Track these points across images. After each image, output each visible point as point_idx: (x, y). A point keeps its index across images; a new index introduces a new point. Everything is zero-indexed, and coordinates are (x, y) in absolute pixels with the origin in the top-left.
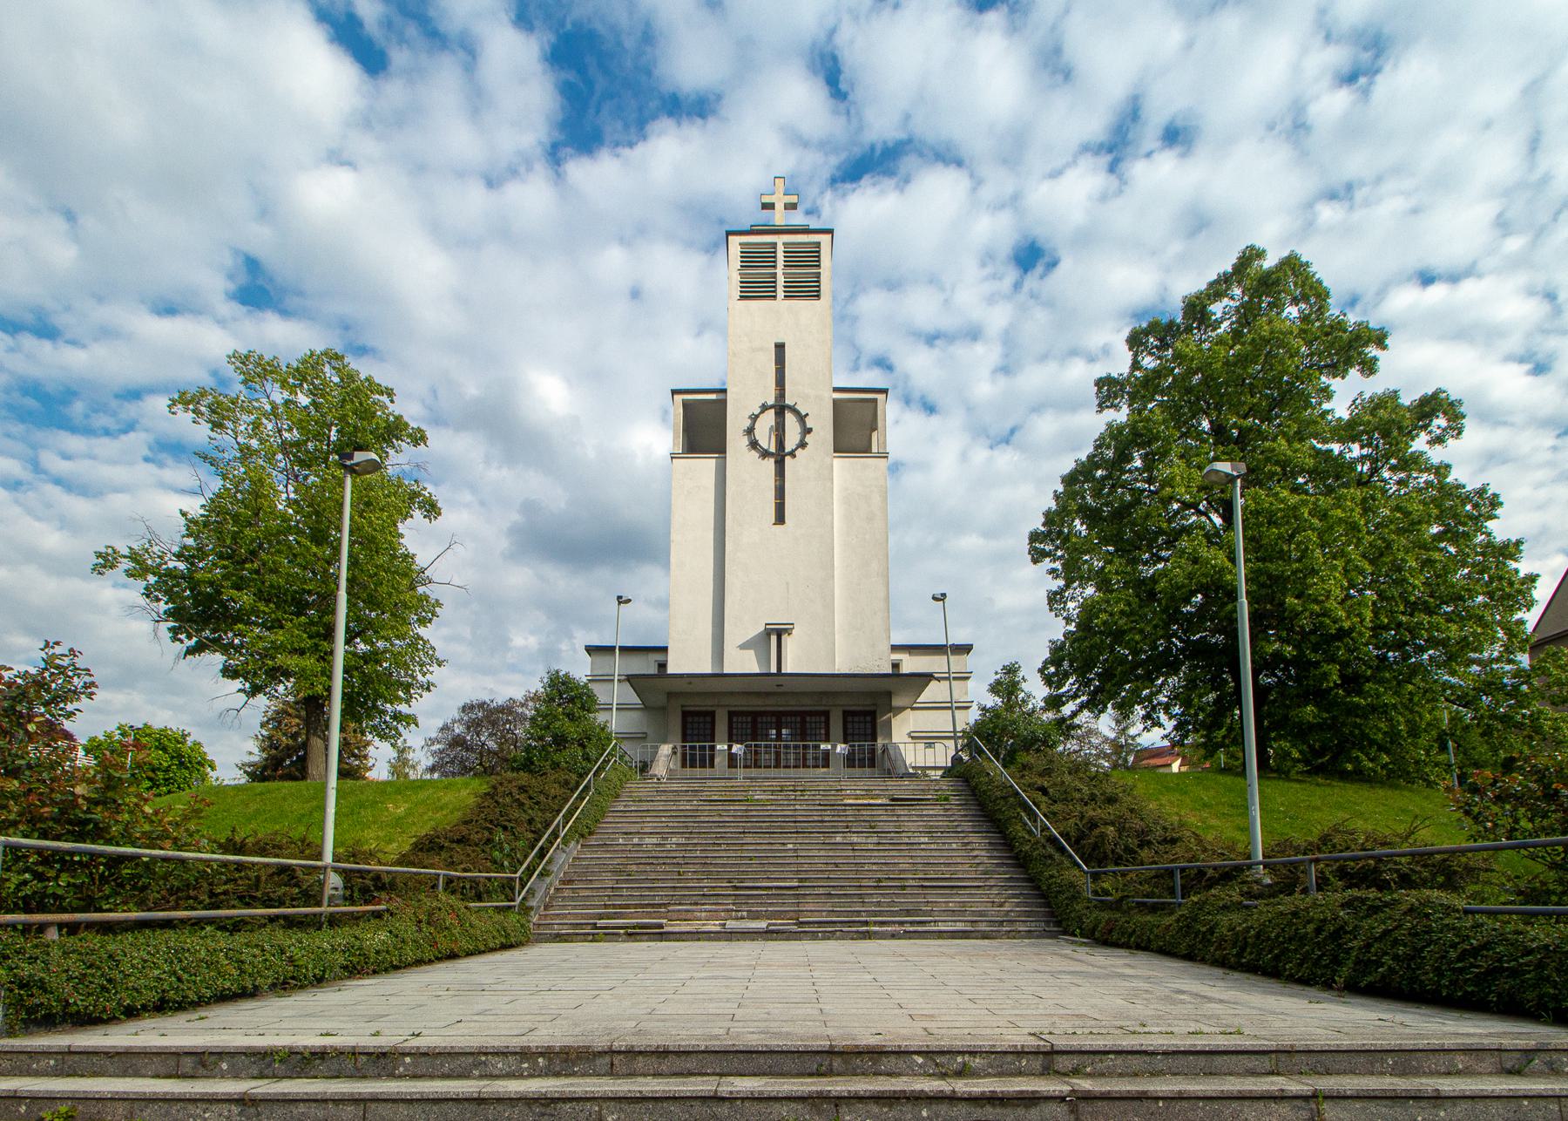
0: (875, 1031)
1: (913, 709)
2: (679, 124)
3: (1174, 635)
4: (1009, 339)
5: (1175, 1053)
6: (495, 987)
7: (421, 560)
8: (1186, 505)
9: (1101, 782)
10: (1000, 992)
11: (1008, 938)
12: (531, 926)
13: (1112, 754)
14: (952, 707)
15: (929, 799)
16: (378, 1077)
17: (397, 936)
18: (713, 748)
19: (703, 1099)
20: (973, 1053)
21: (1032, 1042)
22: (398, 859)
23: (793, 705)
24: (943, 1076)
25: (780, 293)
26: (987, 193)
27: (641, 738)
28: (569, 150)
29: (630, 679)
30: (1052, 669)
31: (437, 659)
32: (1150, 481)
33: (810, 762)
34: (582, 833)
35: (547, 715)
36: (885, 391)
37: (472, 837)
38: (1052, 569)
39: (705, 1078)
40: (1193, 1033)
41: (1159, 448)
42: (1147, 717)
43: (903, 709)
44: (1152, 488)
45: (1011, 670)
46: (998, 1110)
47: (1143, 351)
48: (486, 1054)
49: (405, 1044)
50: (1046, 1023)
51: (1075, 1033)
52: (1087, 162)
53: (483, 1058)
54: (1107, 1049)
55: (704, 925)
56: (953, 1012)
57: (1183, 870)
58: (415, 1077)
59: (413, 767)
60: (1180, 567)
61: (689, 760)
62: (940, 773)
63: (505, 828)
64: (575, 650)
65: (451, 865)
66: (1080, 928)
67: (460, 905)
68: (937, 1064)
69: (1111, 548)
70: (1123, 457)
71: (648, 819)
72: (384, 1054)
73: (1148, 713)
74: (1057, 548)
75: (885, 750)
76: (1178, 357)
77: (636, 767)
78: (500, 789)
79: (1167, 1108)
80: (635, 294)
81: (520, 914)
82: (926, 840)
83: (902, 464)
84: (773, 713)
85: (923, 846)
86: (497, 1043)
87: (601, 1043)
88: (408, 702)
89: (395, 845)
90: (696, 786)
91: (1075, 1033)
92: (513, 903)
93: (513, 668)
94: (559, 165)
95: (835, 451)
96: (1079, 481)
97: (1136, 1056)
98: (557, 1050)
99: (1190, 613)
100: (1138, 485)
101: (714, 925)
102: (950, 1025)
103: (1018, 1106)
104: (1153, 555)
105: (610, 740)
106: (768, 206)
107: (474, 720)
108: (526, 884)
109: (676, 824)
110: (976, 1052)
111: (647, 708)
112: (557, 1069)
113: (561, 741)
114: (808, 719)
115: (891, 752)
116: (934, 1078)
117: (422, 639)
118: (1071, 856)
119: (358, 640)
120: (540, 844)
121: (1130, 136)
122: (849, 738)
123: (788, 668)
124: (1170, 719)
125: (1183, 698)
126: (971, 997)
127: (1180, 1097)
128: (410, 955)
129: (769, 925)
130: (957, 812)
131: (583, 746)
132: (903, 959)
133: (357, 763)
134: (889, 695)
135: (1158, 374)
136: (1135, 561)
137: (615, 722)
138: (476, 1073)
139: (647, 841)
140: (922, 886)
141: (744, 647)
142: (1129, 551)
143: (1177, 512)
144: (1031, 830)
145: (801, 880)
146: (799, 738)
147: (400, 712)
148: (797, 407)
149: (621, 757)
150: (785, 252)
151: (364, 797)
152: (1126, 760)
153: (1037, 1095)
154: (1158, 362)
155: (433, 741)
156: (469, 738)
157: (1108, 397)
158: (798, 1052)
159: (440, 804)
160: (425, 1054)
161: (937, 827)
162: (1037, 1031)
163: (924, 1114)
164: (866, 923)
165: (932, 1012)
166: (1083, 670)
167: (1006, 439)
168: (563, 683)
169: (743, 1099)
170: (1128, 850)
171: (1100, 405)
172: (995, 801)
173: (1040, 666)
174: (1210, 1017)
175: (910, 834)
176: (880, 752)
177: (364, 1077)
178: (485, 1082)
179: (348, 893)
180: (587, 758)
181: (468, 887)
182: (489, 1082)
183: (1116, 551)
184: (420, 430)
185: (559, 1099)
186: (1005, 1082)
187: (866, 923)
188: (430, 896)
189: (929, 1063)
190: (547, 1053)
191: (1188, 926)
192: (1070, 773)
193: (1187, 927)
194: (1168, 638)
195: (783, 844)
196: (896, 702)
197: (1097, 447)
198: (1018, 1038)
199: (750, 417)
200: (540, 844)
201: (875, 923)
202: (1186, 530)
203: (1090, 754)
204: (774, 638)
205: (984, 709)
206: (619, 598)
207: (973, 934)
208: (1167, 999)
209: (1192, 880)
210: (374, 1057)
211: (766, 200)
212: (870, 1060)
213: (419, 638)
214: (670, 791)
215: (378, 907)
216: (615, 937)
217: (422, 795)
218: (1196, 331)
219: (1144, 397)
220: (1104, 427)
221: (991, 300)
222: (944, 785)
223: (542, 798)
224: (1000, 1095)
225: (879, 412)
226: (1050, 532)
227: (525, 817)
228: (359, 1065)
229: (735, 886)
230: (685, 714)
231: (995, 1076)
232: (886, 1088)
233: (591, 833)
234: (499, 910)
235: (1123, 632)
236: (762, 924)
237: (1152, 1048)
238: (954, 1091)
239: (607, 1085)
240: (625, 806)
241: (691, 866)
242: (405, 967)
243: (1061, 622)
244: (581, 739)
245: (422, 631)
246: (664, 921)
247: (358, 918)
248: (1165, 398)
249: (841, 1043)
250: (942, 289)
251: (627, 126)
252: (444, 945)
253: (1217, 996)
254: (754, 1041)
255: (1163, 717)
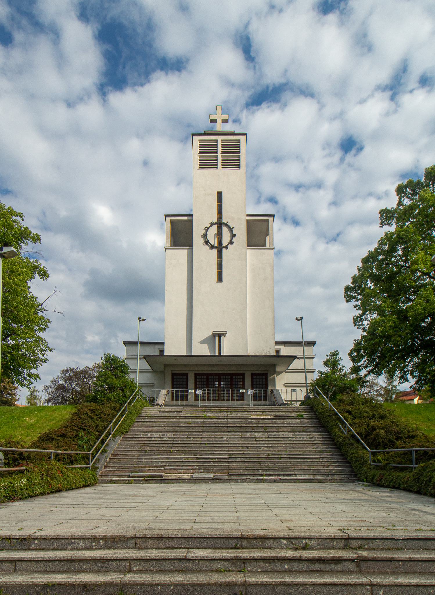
0: (263, 528)
1: (286, 372)
2: (167, 74)
3: (416, 337)
4: (337, 188)
5: (408, 539)
6: (79, 506)
7: (40, 300)
8: (424, 274)
9: (378, 408)
10: (325, 509)
11: (331, 482)
12: (98, 476)
13: (384, 394)
14: (305, 371)
15: (293, 416)
16: (22, 549)
17: (31, 482)
18: (187, 391)
19: (180, 560)
20: (310, 539)
21: (339, 534)
22: (31, 445)
23: (227, 370)
24: (296, 549)
25: (220, 166)
26: (328, 111)
27: (152, 386)
28: (110, 88)
29: (145, 357)
30: (355, 354)
31: (49, 348)
32: (406, 261)
33: (235, 398)
34: (123, 431)
35: (104, 375)
36: (273, 216)
37: (68, 434)
38: (356, 305)
39: (181, 550)
40: (418, 530)
41: (411, 245)
42: (402, 377)
43: (280, 373)
44: (407, 265)
45: (334, 354)
46: (322, 565)
47: (404, 196)
48: (74, 539)
49: (35, 534)
50: (346, 524)
51: (360, 529)
52: (379, 95)
53: (73, 541)
54: (375, 537)
55: (182, 476)
56: (302, 518)
57: (416, 451)
58: (40, 549)
59: (39, 400)
60: (420, 304)
61: (175, 397)
62: (299, 403)
63: (84, 430)
64: (118, 342)
65: (58, 447)
66: (366, 478)
67: (62, 466)
68: (293, 544)
69: (386, 295)
70: (393, 250)
71: (155, 425)
72: (25, 539)
73: (402, 375)
74: (359, 294)
75: (272, 392)
76: (421, 199)
77: (149, 400)
78: (82, 411)
79: (404, 565)
80: (146, 163)
81: (92, 470)
82: (292, 436)
83: (282, 251)
84: (216, 375)
85: (290, 439)
86: (80, 534)
87: (130, 534)
88: (36, 368)
89: (30, 437)
90: (179, 410)
91: (360, 529)
92: (89, 466)
93: (87, 352)
94: (105, 96)
95: (248, 246)
96: (370, 261)
97: (389, 541)
98: (109, 537)
99: (425, 327)
100: (400, 263)
101: (187, 476)
102: (299, 525)
103: (332, 563)
104: (406, 298)
105: (136, 387)
106: (214, 121)
107: (68, 377)
108: (95, 456)
109: (169, 428)
110: (312, 538)
111: (154, 371)
112: (109, 546)
113: (111, 388)
114: (234, 377)
115: (275, 393)
116: (291, 550)
117: (41, 338)
118: (362, 444)
119: (9, 338)
120: (102, 437)
121: (402, 81)
122: (255, 386)
123: (224, 352)
124: (413, 378)
125: (420, 367)
126: (311, 511)
127: (410, 560)
128: (38, 490)
129: (214, 476)
130: (307, 422)
131: (123, 390)
132: (278, 492)
133: (10, 397)
134: (274, 366)
135: (411, 208)
136: (397, 301)
137: (138, 379)
138: (70, 547)
139: (155, 436)
140: (289, 458)
141: (202, 342)
142: (395, 296)
143: (419, 277)
144: (343, 431)
145: (230, 455)
146: (229, 386)
147: (31, 373)
148: (229, 224)
149: (141, 396)
150: (222, 145)
151: (14, 414)
152: (391, 397)
153: (341, 559)
154: (412, 201)
155: (48, 387)
156: (66, 386)
157: (386, 219)
158: (226, 538)
159: (52, 418)
160: (45, 539)
161: (297, 429)
162: (342, 528)
163: (286, 567)
164: (262, 475)
165: (291, 519)
166: (371, 354)
167: (335, 239)
168: (112, 360)
169: (199, 560)
170: (390, 441)
171: (381, 223)
172: (326, 417)
173: (349, 352)
174: (426, 522)
175: (283, 433)
176: (269, 393)
177: (15, 550)
178: (75, 552)
179: (7, 461)
180: (125, 396)
181: (66, 458)
182: (76, 552)
183: (388, 296)
184: (37, 235)
185: (110, 560)
186: (325, 552)
187: (262, 475)
188: (47, 463)
189: (289, 543)
190: (104, 538)
191: (418, 478)
192: (363, 404)
193: (417, 479)
194: (413, 339)
195: (221, 437)
196: (278, 369)
197: (379, 244)
198: (333, 532)
199: (205, 229)
200: (102, 437)
201: (266, 475)
202: (424, 286)
203: (374, 394)
204: (217, 338)
205: (321, 373)
206: (140, 318)
207: (314, 481)
208: (407, 513)
209: (421, 456)
210: (19, 541)
211: (212, 117)
212: (261, 541)
213: (40, 337)
214: (166, 412)
215: (21, 468)
216: (139, 482)
217: (43, 414)
218: (431, 186)
219: (404, 219)
220: (384, 235)
221: (328, 167)
222: (301, 410)
223: (102, 415)
224: (323, 559)
225: (270, 226)
226: (355, 287)
227: (94, 425)
228: (12, 544)
229: (198, 457)
230: (173, 375)
231: (321, 549)
232: (268, 555)
233: (127, 432)
234: (82, 469)
235: (391, 336)
236: (211, 476)
237: (397, 537)
238: (301, 557)
239: (133, 553)
240: (143, 419)
241: (176, 448)
242: (35, 496)
243: (361, 331)
244: (121, 387)
245: (41, 334)
246: (163, 474)
247: (12, 473)
248: (415, 220)
249: (246, 534)
250: (303, 161)
251: (139, 75)
252: (55, 486)
253: (431, 512)
254: (204, 532)
255: (409, 377)
